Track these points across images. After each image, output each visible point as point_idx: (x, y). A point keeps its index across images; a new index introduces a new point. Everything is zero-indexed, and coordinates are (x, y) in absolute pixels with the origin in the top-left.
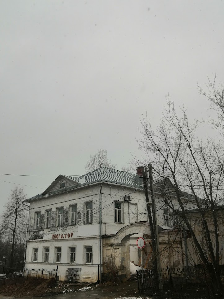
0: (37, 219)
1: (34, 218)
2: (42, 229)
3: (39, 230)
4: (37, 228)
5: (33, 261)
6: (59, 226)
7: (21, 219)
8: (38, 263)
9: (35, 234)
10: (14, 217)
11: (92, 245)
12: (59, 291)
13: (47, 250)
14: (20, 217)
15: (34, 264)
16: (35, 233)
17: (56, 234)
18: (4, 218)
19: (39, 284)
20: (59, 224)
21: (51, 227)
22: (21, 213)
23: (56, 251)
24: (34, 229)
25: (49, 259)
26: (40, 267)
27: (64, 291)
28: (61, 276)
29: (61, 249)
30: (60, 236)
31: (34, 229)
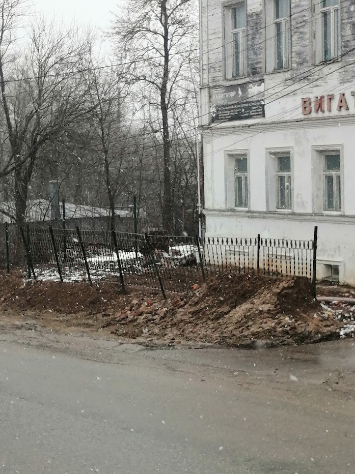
0: (236, 35)
1: (221, 30)
2: (256, 73)
3: (248, 79)
4: (236, 76)
5: (233, 206)
6: (326, 62)
7: (184, 39)
8: (252, 215)
9: (229, 99)
10: (156, 33)
11: (342, 145)
12: (325, 330)
13: (283, 161)
14: (181, 31)
15: (237, 216)
16: (232, 94)
17: (317, 92)
18: (118, 37)
19: (244, 296)
20: (326, 52)
21: (295, 65)
22: (184, 13)
23: (322, 163)
24: (226, 79)
25: (295, 199)
26: (248, 229)
27: (347, 331)
28: (347, 266)
29: (338, 156)
30: (335, 104)
31: (226, 79)
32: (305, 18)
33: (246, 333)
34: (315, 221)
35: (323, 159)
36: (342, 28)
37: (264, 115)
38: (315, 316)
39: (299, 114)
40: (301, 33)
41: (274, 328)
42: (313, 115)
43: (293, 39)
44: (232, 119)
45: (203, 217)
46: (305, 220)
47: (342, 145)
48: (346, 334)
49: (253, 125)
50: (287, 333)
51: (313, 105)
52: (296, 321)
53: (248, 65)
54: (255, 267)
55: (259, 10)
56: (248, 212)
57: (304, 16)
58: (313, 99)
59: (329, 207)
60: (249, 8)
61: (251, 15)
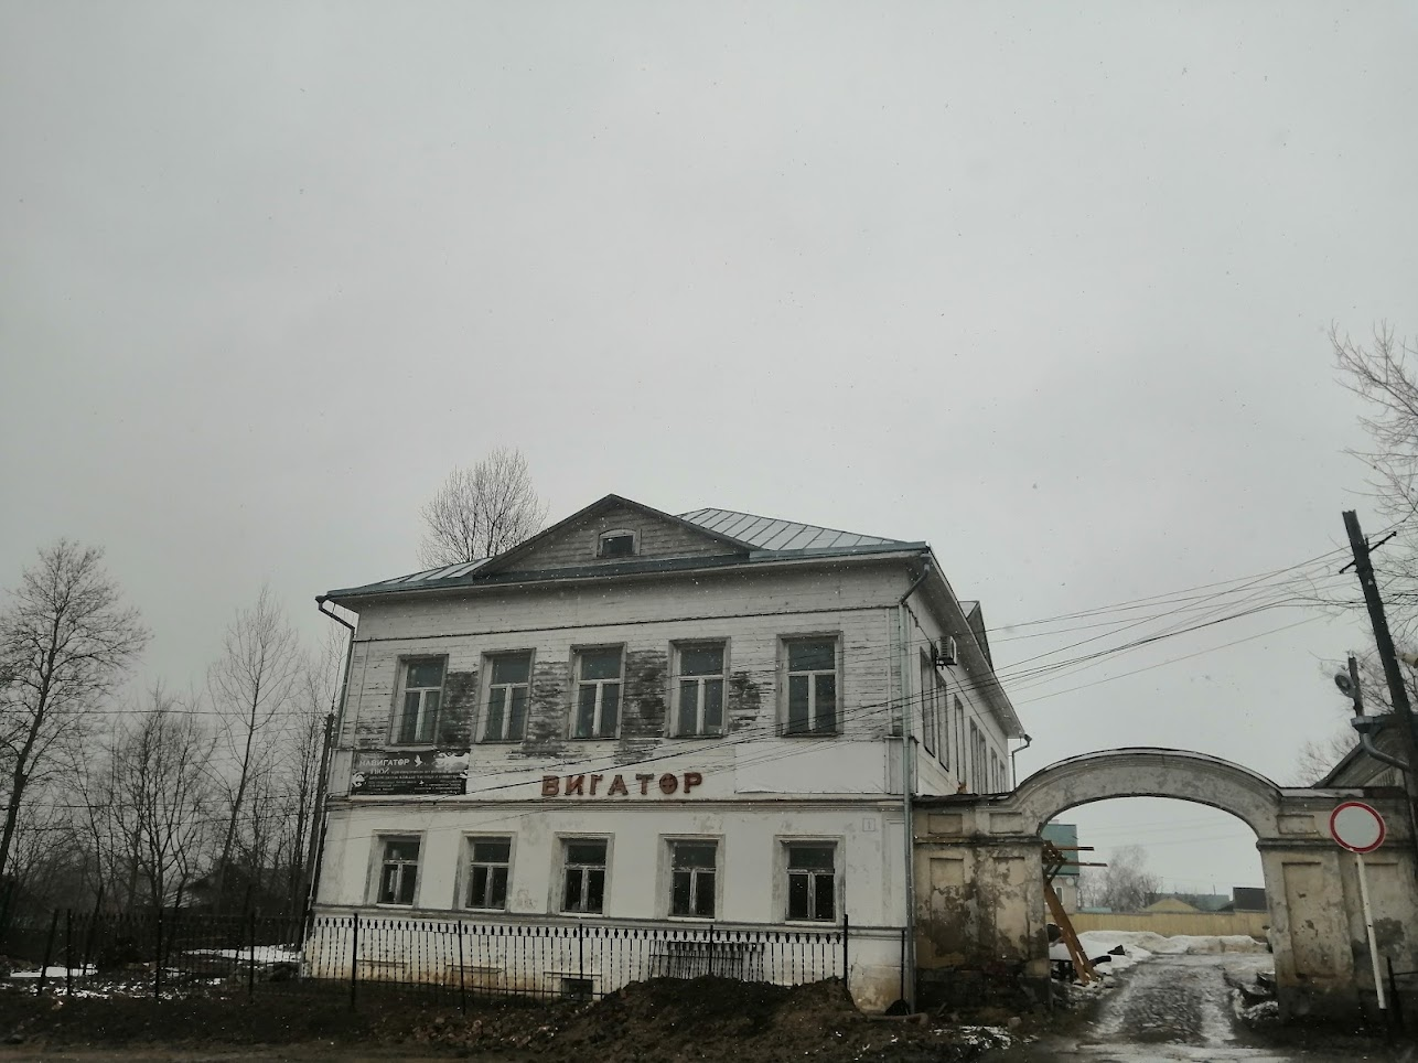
1: (391, 685)
11: (613, 835)
31: (388, 743)
34: (474, 920)
35: (788, 854)
37: (464, 793)
42: (679, 794)
44: (390, 793)
45: (312, 914)
47: (613, 835)
54: (458, 983)
56: (414, 910)
57: (558, 685)
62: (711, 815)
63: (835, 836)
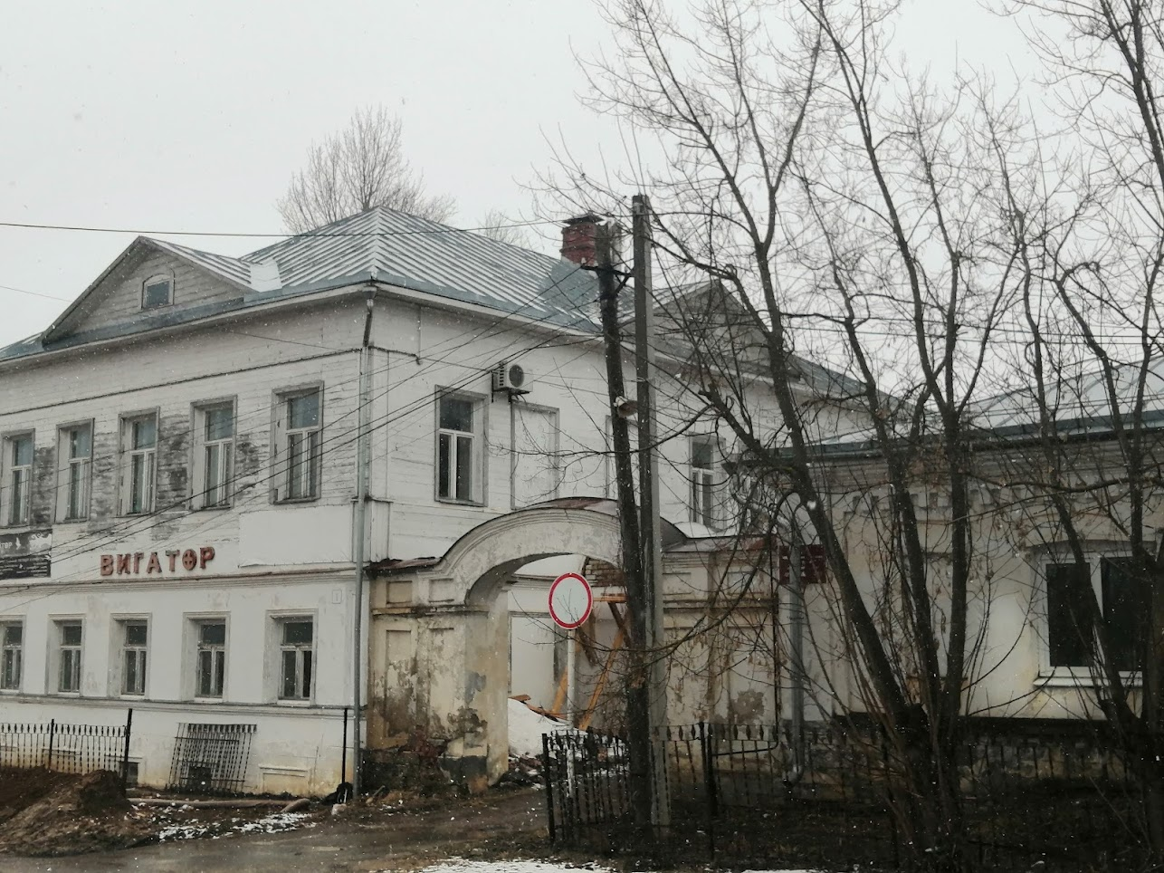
0: (17, 474)
2: (41, 521)
3: (28, 529)
4: (15, 521)
6: (135, 512)
11: (151, 615)
13: (72, 631)
19: (36, 796)
20: (135, 500)
21: (94, 515)
23: (122, 636)
25: (84, 680)
27: (169, 833)
28: (148, 763)
30: (144, 564)
32: (110, 461)
33: (41, 839)
36: (158, 475)
37: (48, 574)
38: (125, 818)
39: (97, 576)
40: (104, 477)
41: (78, 833)
42: (115, 576)
43: (94, 484)
46: (96, 706)
47: (151, 615)
48: (166, 837)
49: (33, 585)
50: (93, 837)
51: (115, 566)
52: (103, 824)
53: (32, 511)
55: (51, 446)
56: (18, 695)
58: (116, 559)
59: (129, 690)
60: (37, 442)
61: (41, 451)
62: (220, 591)
63: (310, 610)
